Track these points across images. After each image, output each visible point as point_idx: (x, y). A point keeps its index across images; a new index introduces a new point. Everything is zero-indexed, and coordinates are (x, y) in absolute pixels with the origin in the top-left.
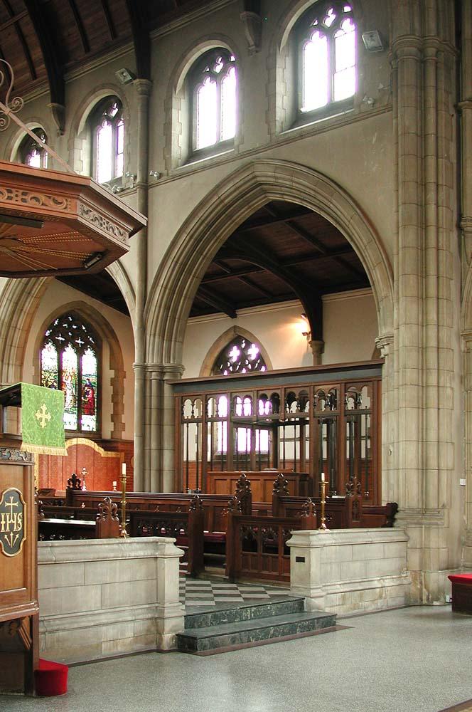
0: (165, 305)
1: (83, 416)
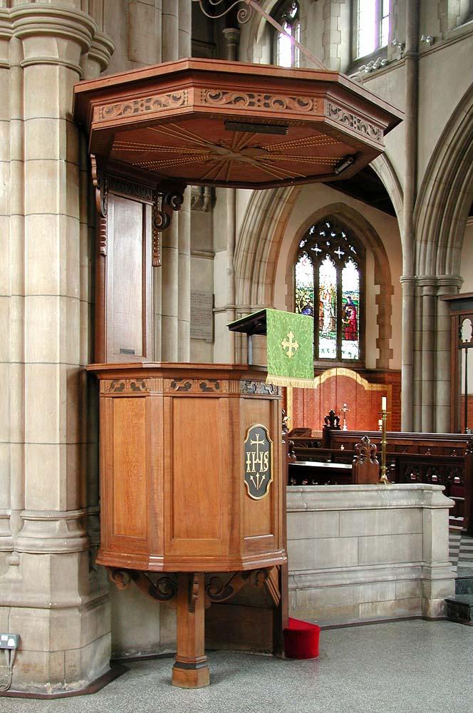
0: (440, 204)
1: (344, 342)
